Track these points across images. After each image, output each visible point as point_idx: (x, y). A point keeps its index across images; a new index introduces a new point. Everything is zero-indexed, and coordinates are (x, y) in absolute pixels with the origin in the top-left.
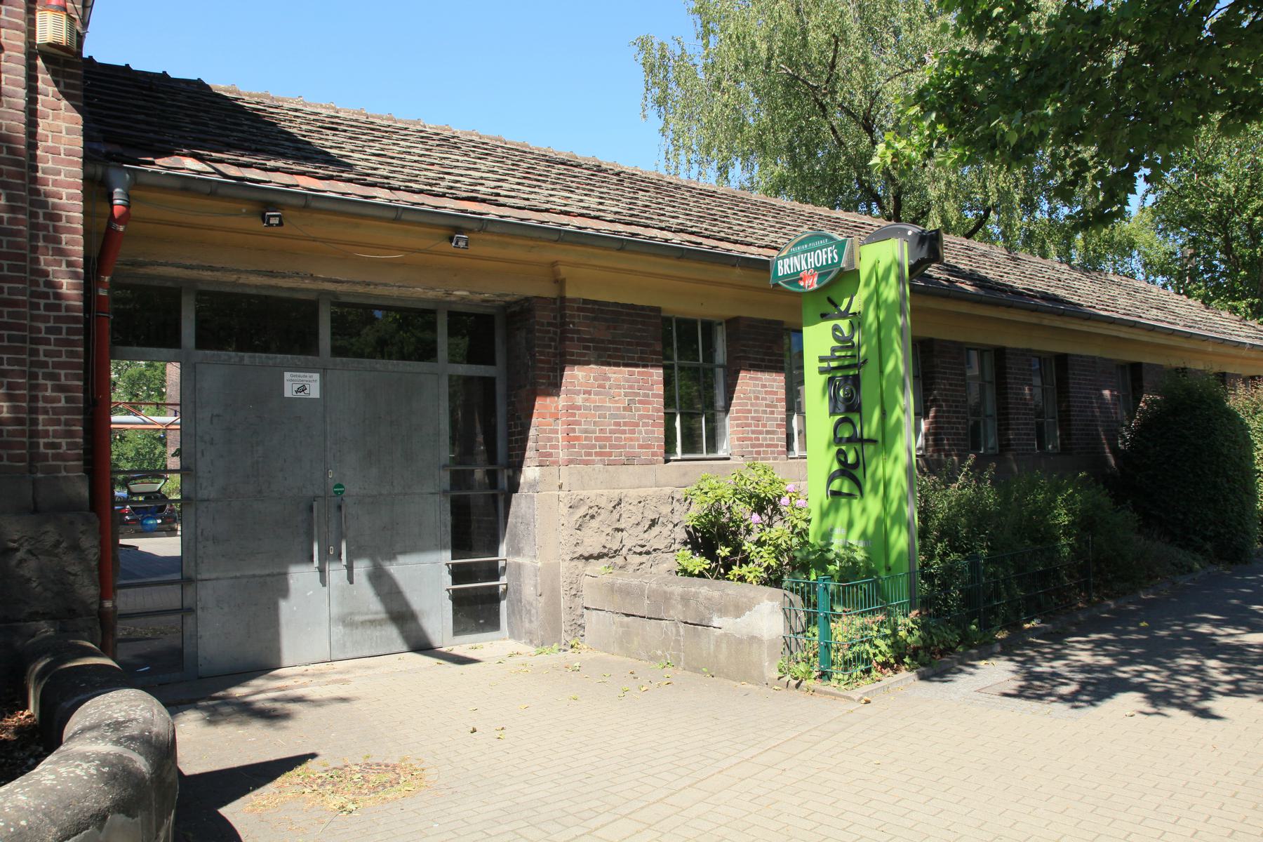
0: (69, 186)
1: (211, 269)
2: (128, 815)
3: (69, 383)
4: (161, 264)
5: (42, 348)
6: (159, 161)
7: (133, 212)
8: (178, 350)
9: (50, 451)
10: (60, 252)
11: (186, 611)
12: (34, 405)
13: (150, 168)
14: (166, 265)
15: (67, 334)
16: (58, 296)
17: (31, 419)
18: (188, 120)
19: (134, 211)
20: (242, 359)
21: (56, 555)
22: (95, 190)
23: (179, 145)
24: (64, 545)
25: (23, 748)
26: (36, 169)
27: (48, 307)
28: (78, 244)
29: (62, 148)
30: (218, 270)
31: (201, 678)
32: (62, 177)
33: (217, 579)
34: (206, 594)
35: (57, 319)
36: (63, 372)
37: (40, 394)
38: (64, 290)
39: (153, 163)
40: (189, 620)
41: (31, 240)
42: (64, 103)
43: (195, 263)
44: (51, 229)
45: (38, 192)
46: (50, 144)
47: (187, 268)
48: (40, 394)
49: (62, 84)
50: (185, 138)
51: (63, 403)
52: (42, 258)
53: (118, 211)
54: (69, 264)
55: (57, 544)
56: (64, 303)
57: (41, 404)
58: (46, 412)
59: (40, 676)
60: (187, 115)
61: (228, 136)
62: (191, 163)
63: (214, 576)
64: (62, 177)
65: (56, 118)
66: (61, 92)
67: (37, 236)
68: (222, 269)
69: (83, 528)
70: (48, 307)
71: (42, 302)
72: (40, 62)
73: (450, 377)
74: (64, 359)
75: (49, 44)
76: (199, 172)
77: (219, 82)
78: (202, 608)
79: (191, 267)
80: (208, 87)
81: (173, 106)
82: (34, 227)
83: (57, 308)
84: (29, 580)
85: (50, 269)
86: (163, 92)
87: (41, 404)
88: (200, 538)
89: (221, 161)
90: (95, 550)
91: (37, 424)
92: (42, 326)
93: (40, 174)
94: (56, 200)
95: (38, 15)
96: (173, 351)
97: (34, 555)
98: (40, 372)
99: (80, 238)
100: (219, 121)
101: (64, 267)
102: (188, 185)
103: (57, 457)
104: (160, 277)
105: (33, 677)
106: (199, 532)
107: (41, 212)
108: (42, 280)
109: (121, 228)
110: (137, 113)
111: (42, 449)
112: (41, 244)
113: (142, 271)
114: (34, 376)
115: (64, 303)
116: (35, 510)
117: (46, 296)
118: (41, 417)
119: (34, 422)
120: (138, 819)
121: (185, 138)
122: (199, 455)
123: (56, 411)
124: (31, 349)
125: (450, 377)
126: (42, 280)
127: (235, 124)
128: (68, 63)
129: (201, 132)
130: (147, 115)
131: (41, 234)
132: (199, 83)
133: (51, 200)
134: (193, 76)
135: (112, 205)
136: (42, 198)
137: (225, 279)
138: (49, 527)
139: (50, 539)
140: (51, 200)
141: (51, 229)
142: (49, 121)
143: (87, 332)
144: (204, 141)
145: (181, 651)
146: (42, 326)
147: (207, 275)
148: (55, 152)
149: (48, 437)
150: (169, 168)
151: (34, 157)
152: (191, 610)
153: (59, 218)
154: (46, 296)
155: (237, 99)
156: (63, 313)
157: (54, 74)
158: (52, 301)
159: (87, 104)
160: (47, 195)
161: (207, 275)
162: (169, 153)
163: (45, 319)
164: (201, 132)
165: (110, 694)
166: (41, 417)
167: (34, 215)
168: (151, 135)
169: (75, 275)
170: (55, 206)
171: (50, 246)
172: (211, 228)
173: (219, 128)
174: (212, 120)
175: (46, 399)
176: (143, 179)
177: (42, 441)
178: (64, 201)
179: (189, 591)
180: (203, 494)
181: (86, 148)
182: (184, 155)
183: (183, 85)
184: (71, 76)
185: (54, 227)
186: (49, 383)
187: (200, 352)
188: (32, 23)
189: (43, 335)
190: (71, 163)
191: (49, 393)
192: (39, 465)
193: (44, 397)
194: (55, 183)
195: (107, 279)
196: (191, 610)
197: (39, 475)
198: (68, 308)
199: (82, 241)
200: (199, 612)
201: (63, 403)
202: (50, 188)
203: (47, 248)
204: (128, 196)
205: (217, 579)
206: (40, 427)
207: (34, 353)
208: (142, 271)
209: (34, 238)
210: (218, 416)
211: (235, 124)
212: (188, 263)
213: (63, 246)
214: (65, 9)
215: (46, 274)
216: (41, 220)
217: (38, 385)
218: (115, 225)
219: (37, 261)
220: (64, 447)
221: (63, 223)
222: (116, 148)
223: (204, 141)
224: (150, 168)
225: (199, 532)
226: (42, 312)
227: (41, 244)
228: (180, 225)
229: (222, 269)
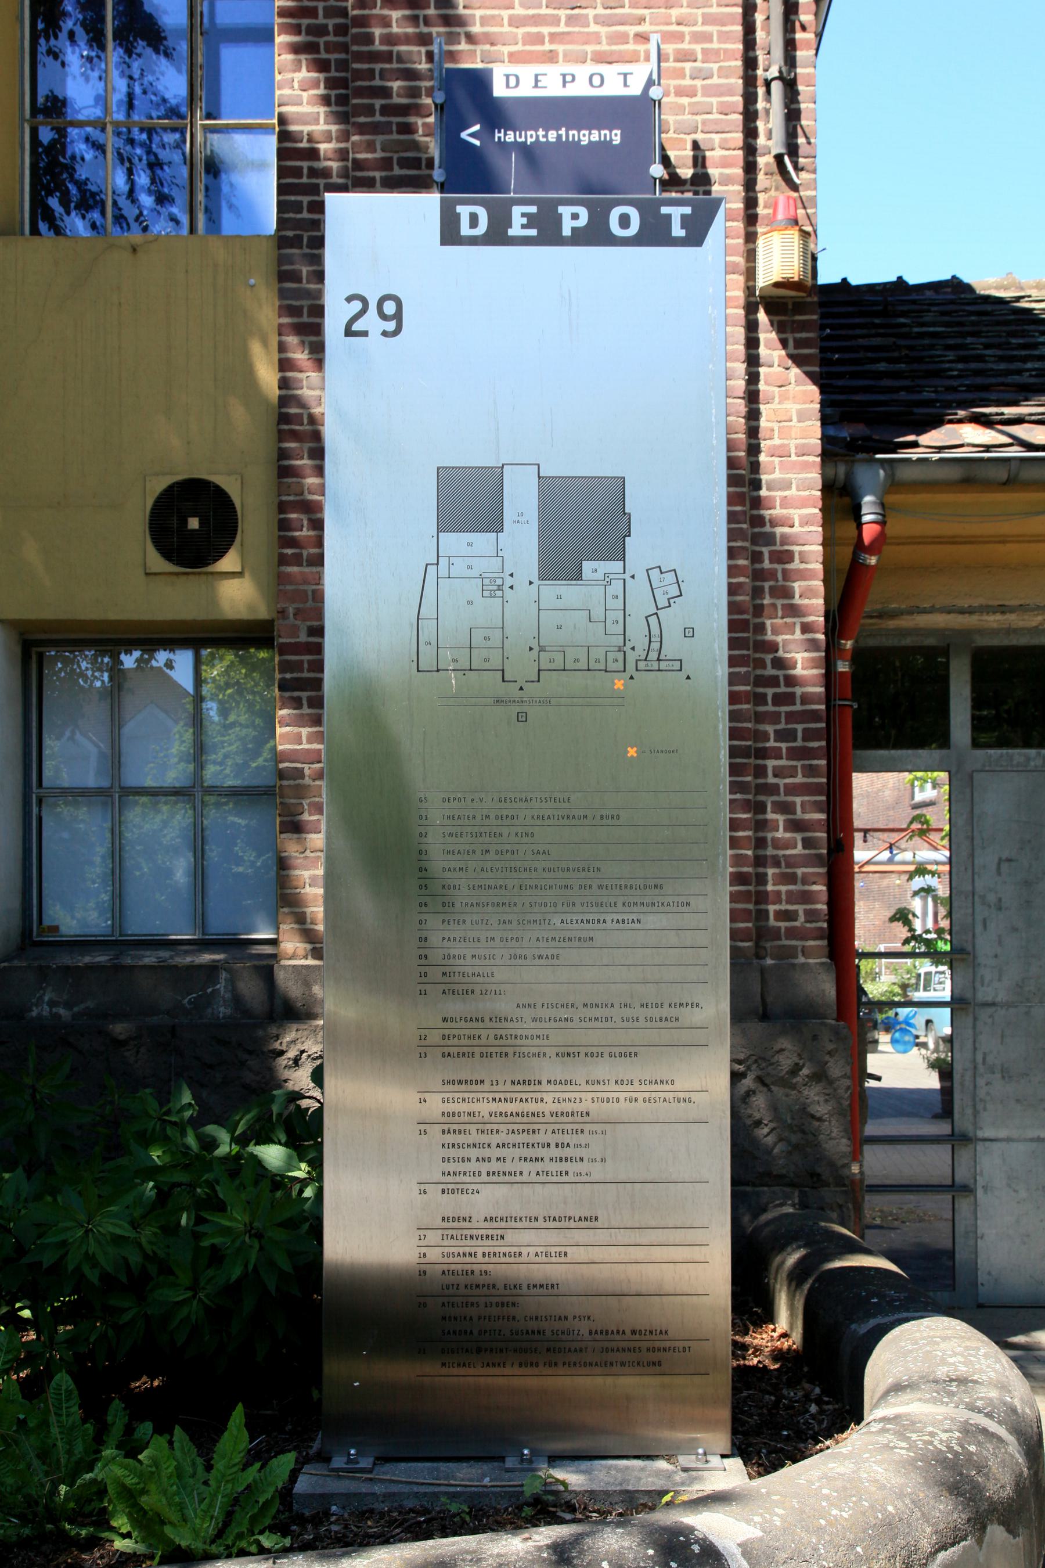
0: (804, 503)
1: (1003, 609)
2: (1009, 1531)
3: (807, 816)
4: (924, 611)
5: (771, 763)
6: (925, 439)
7: (891, 530)
8: (944, 752)
9: (783, 925)
10: (793, 611)
11: (958, 1189)
12: (761, 852)
13: (913, 454)
14: (932, 610)
15: (804, 739)
16: (791, 681)
17: (757, 875)
18: (951, 355)
19: (891, 530)
20: (1011, 758)
21: (793, 1087)
22: (839, 500)
23: (948, 405)
24: (805, 1071)
25: (791, 1384)
26: (757, 485)
27: (778, 700)
28: (816, 597)
29: (792, 444)
30: (1011, 610)
31: (980, 1306)
32: (793, 492)
33: (1008, 1140)
34: (990, 1164)
35: (791, 717)
36: (798, 800)
37: (769, 835)
38: (799, 671)
39: (915, 445)
40: (964, 1205)
41: (753, 598)
42: (795, 372)
43: (976, 603)
44: (780, 576)
45: (759, 521)
46: (777, 441)
47: (962, 612)
48: (769, 835)
49: (791, 343)
50: (954, 389)
51: (799, 850)
52: (768, 623)
53: (869, 533)
54: (806, 628)
55: (795, 1070)
56: (799, 691)
57: (770, 851)
58: (777, 863)
59: (797, 1277)
60: (948, 347)
61: (1019, 372)
62: (973, 435)
63: (1002, 1134)
64: (793, 492)
65: (783, 399)
66: (790, 356)
67: (762, 588)
68: (1022, 608)
69: (831, 1047)
70: (778, 700)
71: (770, 692)
72: (762, 316)
73: (976, 744)
74: (799, 779)
75: (777, 285)
76: (988, 448)
77: (986, 278)
78: (985, 1188)
79: (970, 611)
80: (968, 288)
81: (921, 335)
82: (759, 575)
83: (787, 699)
84: (758, 1123)
85: (780, 639)
86: (904, 314)
87: (770, 851)
88: (981, 1069)
89: (1019, 421)
90: (848, 1082)
91: (765, 883)
92: (770, 729)
93: (763, 493)
94: (786, 530)
95: (761, 242)
96: (933, 754)
97: (765, 1084)
98: (769, 801)
99: (818, 584)
100: (999, 346)
101: (798, 634)
102: (972, 474)
103: (792, 933)
104: (917, 631)
105: (783, 1275)
106: (979, 1058)
107: (766, 551)
108: (768, 658)
109: (873, 561)
110: (878, 360)
111: (772, 922)
112: (767, 601)
113: (892, 624)
114: (760, 808)
115: (799, 691)
116: (765, 1016)
117: (773, 681)
118: (770, 871)
119: (762, 879)
120: (1020, 1540)
121: (954, 389)
122: (979, 928)
123: (790, 862)
124: (757, 767)
125: (976, 744)
126: (768, 658)
127: (1025, 347)
128: (799, 307)
129: (977, 373)
130: (890, 361)
131: (767, 585)
132: (956, 287)
133: (779, 530)
134: (942, 274)
135: (860, 525)
136: (767, 529)
137: (1021, 624)
138: (784, 1043)
139: (786, 1062)
140: (779, 530)
141: (780, 576)
142: (774, 406)
143: (828, 734)
144: (986, 388)
145: (951, 1254)
146: (770, 729)
147: (993, 620)
148: (782, 453)
149: (780, 902)
150: (940, 449)
151: (755, 467)
152: (967, 1190)
153: (789, 557)
154: (773, 681)
155: (1018, 299)
156: (798, 707)
157: (780, 328)
158: (783, 689)
159: (824, 362)
160: (774, 523)
161: (993, 620)
162: (936, 422)
163: (775, 718)
164: (977, 373)
165: (926, 1321)
166: (770, 871)
167: (756, 557)
168: (903, 395)
169: (813, 645)
170: (785, 540)
171: (779, 602)
172: (1003, 540)
173: (1002, 359)
174: (987, 347)
175: (777, 844)
176: (905, 474)
177: (772, 908)
178: (797, 529)
179: (964, 1155)
180: (984, 994)
181: (825, 439)
182: (960, 421)
183: (929, 294)
184: (803, 326)
185: (784, 571)
186: (781, 818)
187: (980, 753)
188: (751, 255)
189: (772, 743)
190: (806, 467)
191: (780, 834)
192: (768, 945)
193: (773, 839)
194: (785, 503)
195: (849, 644)
196: (967, 1190)
197: (769, 961)
198: (806, 699)
199: (822, 589)
200: (980, 1192)
201: (799, 850)
202: (777, 512)
203: (774, 606)
204: (882, 505)
205: (1008, 1140)
206: (770, 888)
207: (760, 771)
208: (892, 624)
209: (757, 592)
210: (1009, 860)
211: (1025, 347)
212: (965, 603)
213: (797, 600)
214: (796, 222)
215: (773, 647)
216: (767, 564)
217: (766, 821)
218: (863, 556)
219: (761, 628)
220: (802, 918)
221: (796, 565)
222: (860, 429)
223: (986, 388)
224: (913, 454)
225: (979, 1058)
226: (770, 708)
227: (767, 601)
228: (953, 540)
229: (1022, 608)
